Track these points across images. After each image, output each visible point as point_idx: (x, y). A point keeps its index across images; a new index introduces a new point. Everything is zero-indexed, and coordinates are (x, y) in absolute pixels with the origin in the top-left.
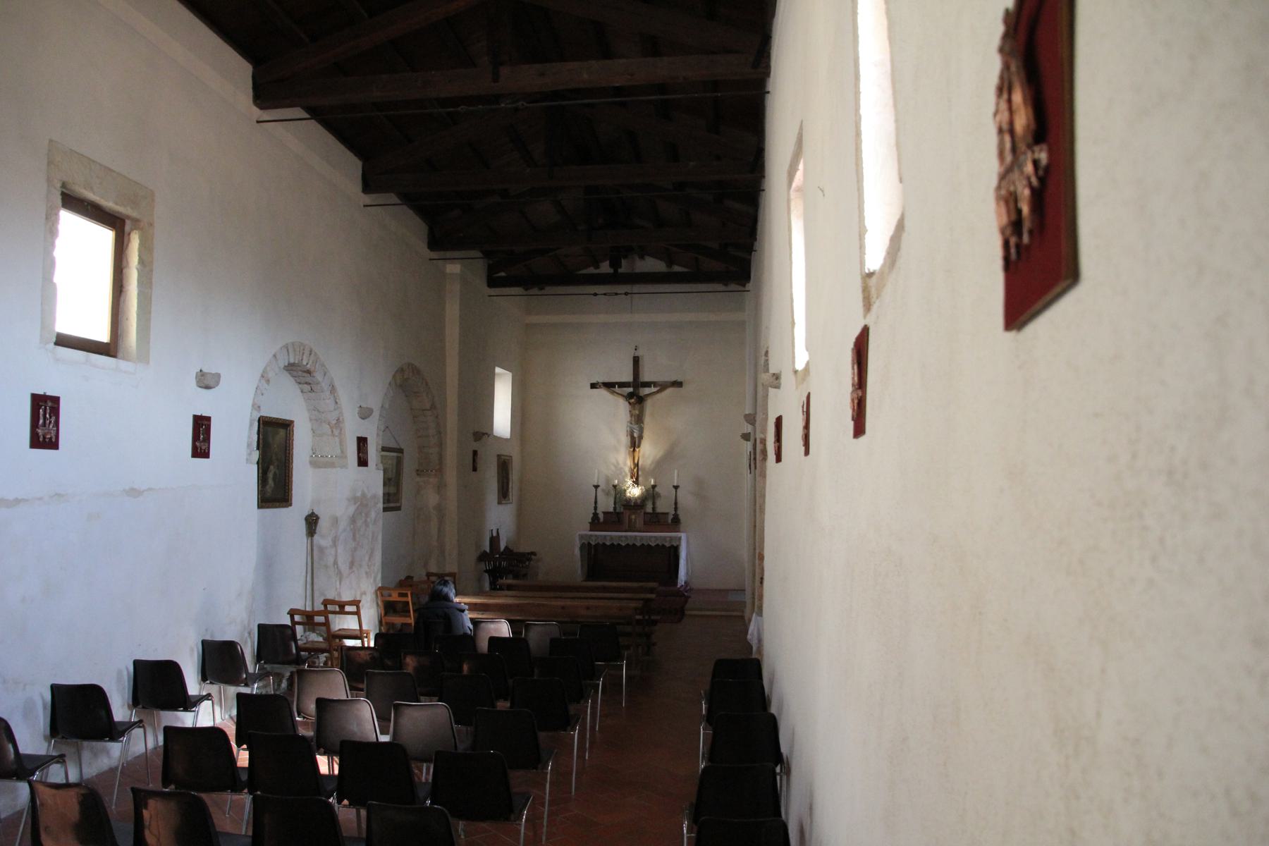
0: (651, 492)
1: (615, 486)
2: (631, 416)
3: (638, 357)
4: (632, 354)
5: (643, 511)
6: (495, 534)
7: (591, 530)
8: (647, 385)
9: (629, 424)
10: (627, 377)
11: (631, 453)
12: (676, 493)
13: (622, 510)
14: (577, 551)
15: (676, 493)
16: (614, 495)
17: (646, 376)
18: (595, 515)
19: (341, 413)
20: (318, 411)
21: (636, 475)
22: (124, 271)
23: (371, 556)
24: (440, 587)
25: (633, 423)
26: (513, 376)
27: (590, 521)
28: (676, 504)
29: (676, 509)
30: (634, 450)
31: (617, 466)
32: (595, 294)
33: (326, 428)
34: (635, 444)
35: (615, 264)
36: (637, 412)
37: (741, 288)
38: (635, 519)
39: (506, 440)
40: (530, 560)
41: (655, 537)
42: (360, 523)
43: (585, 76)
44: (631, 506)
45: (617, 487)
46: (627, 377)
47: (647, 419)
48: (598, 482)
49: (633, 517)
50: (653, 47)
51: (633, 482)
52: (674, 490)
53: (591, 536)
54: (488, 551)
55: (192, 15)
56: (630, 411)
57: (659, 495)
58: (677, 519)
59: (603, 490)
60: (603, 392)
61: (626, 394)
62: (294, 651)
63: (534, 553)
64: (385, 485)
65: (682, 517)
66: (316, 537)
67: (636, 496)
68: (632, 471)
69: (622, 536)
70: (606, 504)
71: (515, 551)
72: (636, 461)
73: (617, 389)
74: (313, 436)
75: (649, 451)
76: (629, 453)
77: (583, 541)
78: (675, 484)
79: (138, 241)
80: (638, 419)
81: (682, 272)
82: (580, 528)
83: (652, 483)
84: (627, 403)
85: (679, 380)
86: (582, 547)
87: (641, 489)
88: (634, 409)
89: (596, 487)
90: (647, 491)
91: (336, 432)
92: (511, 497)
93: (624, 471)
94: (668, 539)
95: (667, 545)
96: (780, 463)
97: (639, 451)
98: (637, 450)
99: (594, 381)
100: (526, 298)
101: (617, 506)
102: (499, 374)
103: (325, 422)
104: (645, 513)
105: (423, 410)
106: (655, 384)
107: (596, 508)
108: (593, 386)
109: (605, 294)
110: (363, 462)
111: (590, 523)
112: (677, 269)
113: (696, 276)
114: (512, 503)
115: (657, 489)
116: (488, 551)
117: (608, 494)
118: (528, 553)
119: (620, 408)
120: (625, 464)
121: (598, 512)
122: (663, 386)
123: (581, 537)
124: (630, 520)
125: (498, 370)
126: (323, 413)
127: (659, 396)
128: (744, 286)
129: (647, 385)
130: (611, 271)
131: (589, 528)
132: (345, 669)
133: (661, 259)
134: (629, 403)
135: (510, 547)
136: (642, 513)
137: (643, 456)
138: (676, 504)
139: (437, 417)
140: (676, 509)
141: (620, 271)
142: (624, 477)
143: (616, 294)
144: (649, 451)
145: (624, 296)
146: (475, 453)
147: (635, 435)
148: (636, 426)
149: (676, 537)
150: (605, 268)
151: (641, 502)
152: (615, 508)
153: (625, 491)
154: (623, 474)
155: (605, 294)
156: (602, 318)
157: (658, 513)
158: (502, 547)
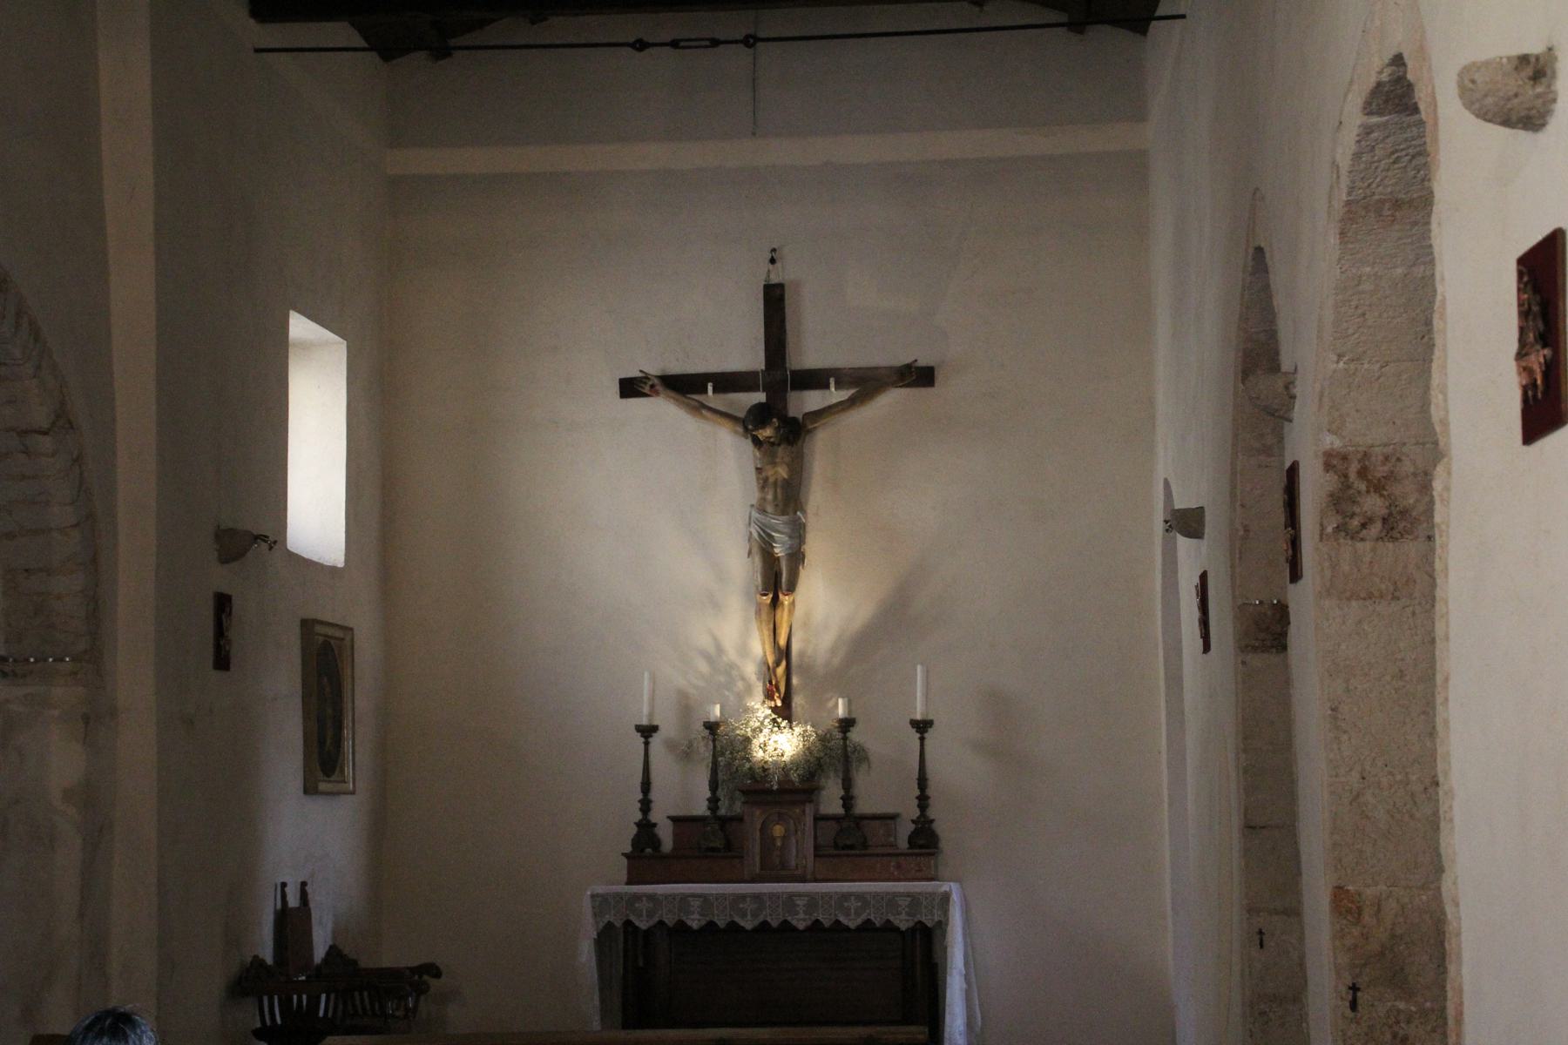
1: (712, 727)
2: (764, 484)
3: (781, 286)
5: (809, 809)
6: (293, 901)
7: (629, 882)
8: (814, 379)
9: (755, 514)
10: (747, 355)
11: (765, 610)
12: (922, 745)
13: (738, 808)
14: (586, 952)
15: (922, 745)
16: (708, 755)
17: (809, 353)
18: (646, 829)
21: (783, 689)
25: (770, 509)
26: (348, 347)
28: (922, 782)
29: (923, 801)
30: (775, 602)
31: (714, 657)
32: (641, 45)
36: (783, 472)
38: (785, 838)
39: (333, 570)
40: (421, 990)
41: (860, 896)
44: (770, 792)
46: (747, 355)
47: (817, 497)
48: (651, 715)
49: (778, 830)
51: (775, 710)
53: (637, 897)
54: (269, 960)
56: (759, 470)
57: (862, 755)
58: (925, 839)
59: (671, 745)
60: (663, 409)
61: (742, 415)
63: (433, 970)
65: (940, 827)
67: (786, 758)
68: (768, 672)
69: (743, 897)
71: (365, 962)
72: (782, 642)
73: (710, 397)
76: (758, 612)
77: (607, 918)
83: (841, 711)
84: (747, 445)
85: (922, 362)
86: (604, 938)
87: (804, 735)
88: (774, 464)
89: (647, 731)
90: (823, 739)
92: (348, 771)
93: (743, 679)
94: (904, 902)
95: (903, 922)
97: (793, 604)
98: (786, 600)
99: (633, 373)
101: (720, 793)
102: (307, 346)
104: (819, 818)
105: (24, 433)
106: (841, 377)
107: (646, 805)
108: (630, 388)
109: (675, 44)
111: (708, 800)
114: (353, 793)
115: (855, 735)
116: (269, 960)
117: (686, 754)
118: (413, 970)
120: (744, 650)
123: (601, 903)
124: (767, 841)
125: (300, 327)
129: (814, 379)
131: (624, 875)
132: (1427, 499)
134: (757, 442)
135: (347, 950)
136: (809, 820)
137: (806, 625)
138: (922, 782)
139: (78, 460)
140: (923, 801)
142: (740, 697)
143: (715, 43)
146: (223, 603)
147: (779, 551)
148: (778, 521)
149: (931, 895)
151: (803, 779)
152: (713, 802)
154: (740, 685)
156: (652, 155)
157: (864, 817)
158: (319, 953)
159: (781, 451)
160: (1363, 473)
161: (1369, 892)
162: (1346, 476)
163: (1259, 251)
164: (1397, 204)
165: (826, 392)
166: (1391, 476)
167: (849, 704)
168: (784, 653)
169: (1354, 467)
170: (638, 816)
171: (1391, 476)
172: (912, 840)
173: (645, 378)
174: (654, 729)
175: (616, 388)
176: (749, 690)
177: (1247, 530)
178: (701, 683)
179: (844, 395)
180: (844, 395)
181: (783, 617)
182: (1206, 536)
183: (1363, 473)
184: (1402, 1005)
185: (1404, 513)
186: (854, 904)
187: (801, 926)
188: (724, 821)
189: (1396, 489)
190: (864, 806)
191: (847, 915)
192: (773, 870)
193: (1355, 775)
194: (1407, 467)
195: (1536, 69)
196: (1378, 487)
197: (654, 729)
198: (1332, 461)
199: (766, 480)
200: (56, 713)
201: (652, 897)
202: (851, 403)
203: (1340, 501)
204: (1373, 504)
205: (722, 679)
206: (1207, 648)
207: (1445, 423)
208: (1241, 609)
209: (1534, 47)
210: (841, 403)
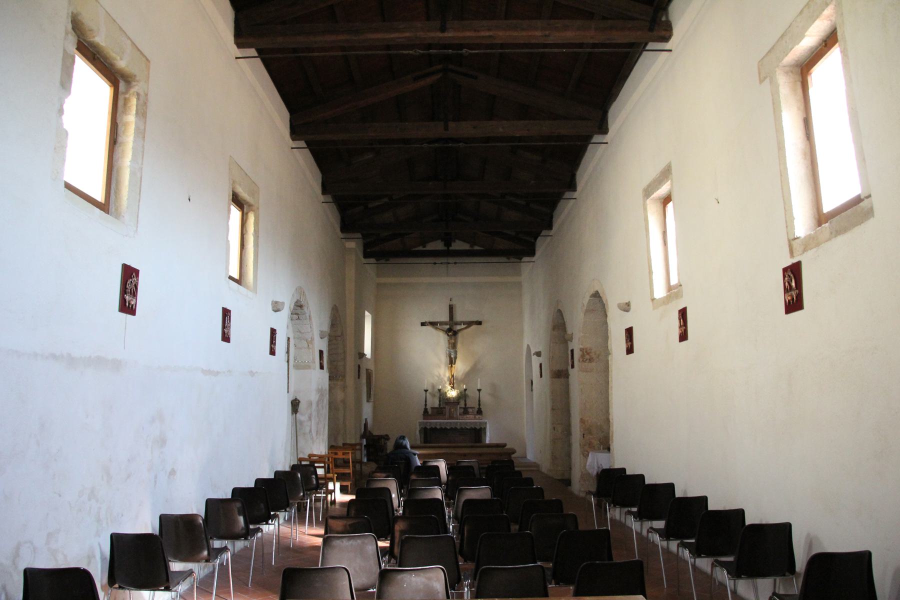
0: (464, 393)
1: (439, 390)
2: (449, 343)
4: (448, 302)
9: (448, 349)
13: (444, 406)
18: (426, 411)
19: (313, 334)
20: (300, 332)
22: (244, 236)
23: (324, 428)
24: (401, 441)
25: (450, 348)
27: (423, 413)
28: (479, 401)
29: (479, 405)
30: (452, 366)
33: (305, 344)
34: (452, 362)
35: (448, 244)
36: (453, 341)
37: (519, 261)
38: (454, 411)
42: (320, 406)
43: (501, 130)
45: (442, 391)
46: (445, 318)
47: (459, 346)
48: (427, 388)
49: (452, 410)
50: (524, 112)
51: (451, 387)
52: (478, 392)
55: (274, 86)
56: (449, 341)
58: (480, 412)
59: (430, 393)
60: (429, 328)
61: (446, 330)
62: (315, 482)
64: (330, 379)
66: (298, 415)
67: (454, 396)
68: (450, 380)
70: (434, 402)
74: (295, 349)
75: (461, 367)
77: (422, 426)
78: (479, 388)
79: (254, 218)
80: (453, 346)
81: (479, 250)
82: (416, 421)
89: (426, 391)
90: (461, 393)
91: (310, 346)
94: (478, 424)
96: (573, 369)
98: (454, 366)
100: (376, 265)
101: (441, 403)
103: (303, 339)
104: (460, 408)
106: (464, 323)
107: (426, 405)
108: (423, 324)
109: (441, 263)
110: (322, 367)
112: (476, 248)
113: (489, 252)
115: (466, 392)
117: (433, 395)
119: (441, 339)
120: (445, 375)
121: (427, 407)
122: (469, 324)
123: (420, 424)
126: (303, 333)
127: (465, 331)
128: (521, 259)
130: (446, 248)
133: (468, 243)
134: (448, 335)
136: (458, 408)
138: (479, 401)
140: (479, 405)
141: (451, 248)
144: (461, 367)
145: (453, 264)
147: (452, 356)
148: (452, 351)
150: (438, 245)
152: (440, 405)
153: (446, 393)
154: (444, 382)
155: (441, 263)
159: (453, 337)
160: (586, 352)
161: (586, 419)
162: (583, 352)
163: (560, 311)
166: (590, 352)
167: (466, 386)
168: (453, 376)
169: (585, 351)
170: (424, 407)
173: (426, 322)
176: (445, 383)
179: (464, 326)
180: (464, 326)
181: (453, 369)
182: (542, 356)
183: (586, 352)
184: (591, 437)
188: (441, 408)
189: (591, 354)
192: (451, 417)
194: (593, 351)
195: (628, 304)
196: (588, 354)
198: (581, 350)
200: (339, 387)
201: (430, 423)
202: (466, 328)
203: (583, 356)
204: (587, 357)
206: (541, 376)
207: (611, 349)
208: (551, 371)
209: (627, 302)
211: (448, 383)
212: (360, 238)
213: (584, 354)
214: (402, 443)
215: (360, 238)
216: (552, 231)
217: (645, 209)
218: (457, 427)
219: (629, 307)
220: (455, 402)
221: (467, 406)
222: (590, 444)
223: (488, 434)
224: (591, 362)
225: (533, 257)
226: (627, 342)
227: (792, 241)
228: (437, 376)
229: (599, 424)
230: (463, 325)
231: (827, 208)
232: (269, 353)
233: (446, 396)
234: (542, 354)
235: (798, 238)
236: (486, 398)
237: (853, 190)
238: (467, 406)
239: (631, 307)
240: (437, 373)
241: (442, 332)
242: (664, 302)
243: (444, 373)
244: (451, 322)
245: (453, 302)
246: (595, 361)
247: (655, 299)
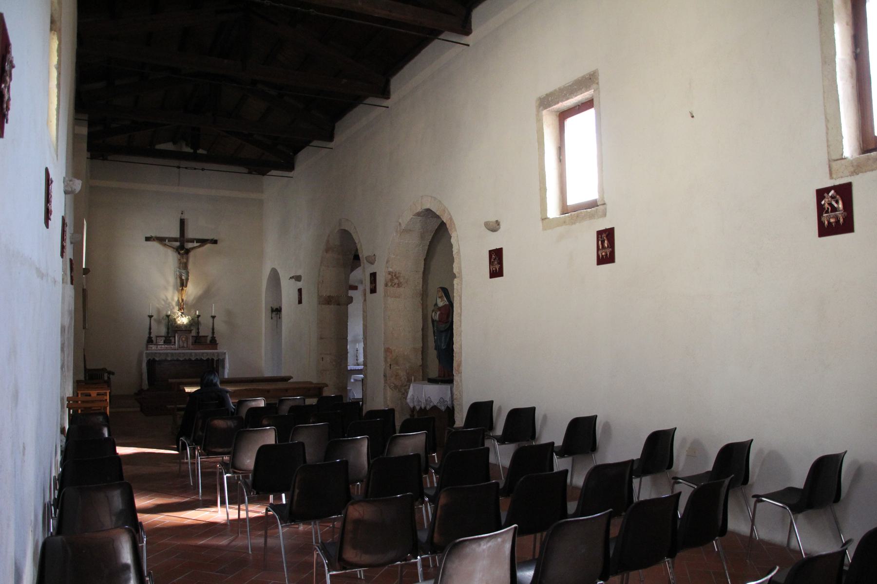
1: (168, 316)
3: (184, 219)
4: (179, 216)
8: (192, 241)
9: (178, 269)
28: (213, 329)
29: (213, 333)
30: (182, 289)
31: (166, 300)
36: (185, 260)
41: (207, 353)
46: (176, 234)
47: (190, 266)
51: (182, 312)
56: (179, 260)
59: (155, 320)
60: (156, 245)
67: (185, 323)
75: (192, 290)
77: (150, 358)
80: (184, 266)
89: (151, 317)
90: (192, 319)
93: (172, 305)
104: (192, 336)
106: (198, 241)
107: (150, 333)
108: (148, 239)
109: (186, 168)
115: (200, 319)
119: (169, 258)
120: (173, 300)
122: (203, 242)
134: (179, 253)
140: (213, 333)
143: (195, 169)
144: (192, 290)
147: (183, 278)
148: (184, 271)
153: (175, 319)
157: (201, 337)
159: (184, 256)
160: (395, 275)
162: (392, 276)
164: (410, 231)
165: (193, 244)
166: (399, 277)
167: (199, 312)
169: (394, 275)
170: (147, 335)
171: (399, 277)
172: (211, 341)
174: (152, 316)
175: (144, 239)
176: (173, 308)
177: (323, 281)
178: (162, 306)
180: (198, 244)
183: (395, 275)
184: (398, 367)
185: (401, 283)
186: (205, 355)
187: (193, 359)
190: (201, 334)
191: (204, 357)
193: (392, 329)
196: (397, 278)
197: (152, 316)
199: (181, 262)
204: (396, 281)
205: (167, 305)
206: (300, 302)
210: (197, 246)
211: (177, 308)
212: (85, 120)
213: (392, 278)
214: (212, 380)
215: (85, 120)
216: (333, 143)
217: (539, 120)
218: (191, 358)
219: (498, 227)
220: (186, 329)
221: (200, 335)
222: (396, 376)
223: (227, 365)
224: (399, 287)
225: (291, 171)
226: (491, 263)
227: (835, 160)
228: (163, 300)
229: (406, 354)
230: (196, 242)
231: (571, 201)
232: (598, 230)
233: (176, 323)
234: (303, 278)
235: (845, 158)
236: (220, 326)
237: (592, 195)
238: (200, 335)
239: (501, 227)
240: (163, 297)
241: (172, 249)
242: (565, 222)
243: (172, 296)
244: (182, 239)
245: (185, 216)
246: (403, 286)
247: (547, 218)
